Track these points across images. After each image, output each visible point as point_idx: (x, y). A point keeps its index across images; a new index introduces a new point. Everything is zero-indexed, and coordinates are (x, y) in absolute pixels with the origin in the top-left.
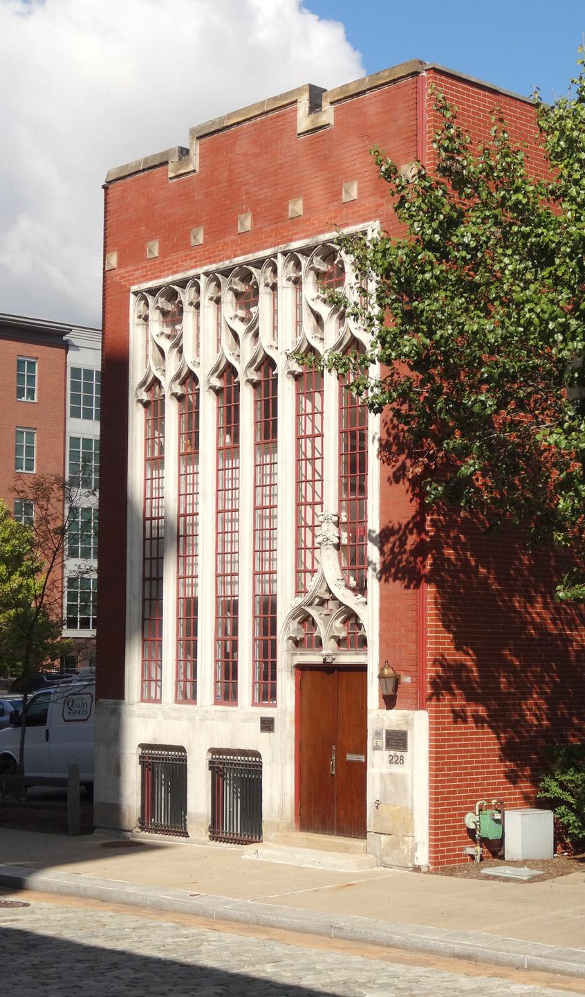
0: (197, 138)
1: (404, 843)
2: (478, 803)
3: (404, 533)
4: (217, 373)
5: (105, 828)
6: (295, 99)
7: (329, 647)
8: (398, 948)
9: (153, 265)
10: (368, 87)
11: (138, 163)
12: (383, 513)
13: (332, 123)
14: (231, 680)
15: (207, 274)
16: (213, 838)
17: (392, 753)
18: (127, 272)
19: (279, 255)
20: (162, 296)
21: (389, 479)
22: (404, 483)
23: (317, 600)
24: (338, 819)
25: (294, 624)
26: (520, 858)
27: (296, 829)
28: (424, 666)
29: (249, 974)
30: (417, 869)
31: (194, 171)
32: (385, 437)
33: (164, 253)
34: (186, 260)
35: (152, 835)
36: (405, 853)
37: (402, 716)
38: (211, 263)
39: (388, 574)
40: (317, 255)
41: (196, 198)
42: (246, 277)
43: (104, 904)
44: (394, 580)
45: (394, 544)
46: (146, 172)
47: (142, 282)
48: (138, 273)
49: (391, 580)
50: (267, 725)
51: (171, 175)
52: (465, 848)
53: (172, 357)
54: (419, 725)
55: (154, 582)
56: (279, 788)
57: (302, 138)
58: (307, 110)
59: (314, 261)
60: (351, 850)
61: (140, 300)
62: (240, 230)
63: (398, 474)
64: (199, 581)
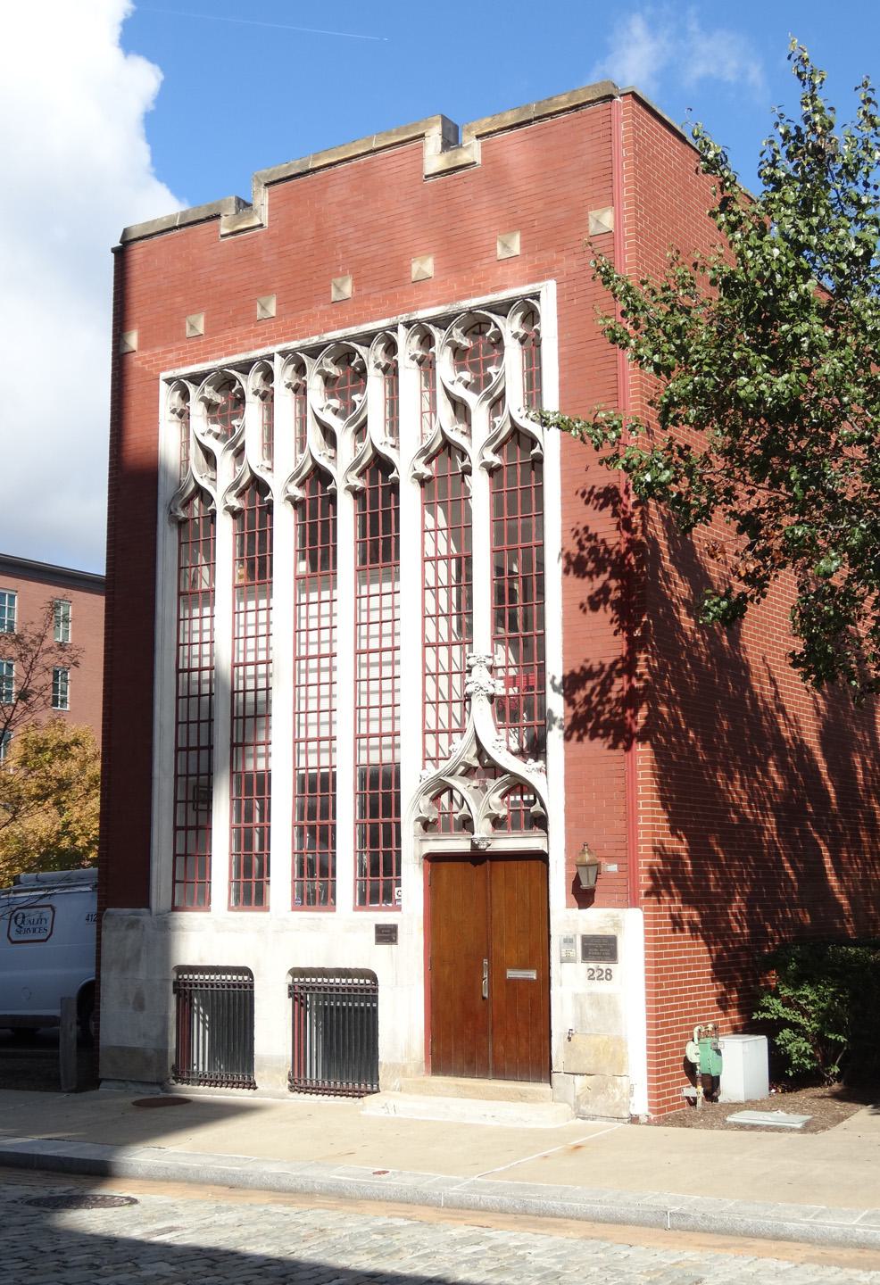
0: (266, 185)
1: (615, 1085)
2: (696, 1029)
3: (609, 676)
4: (297, 480)
5: (119, 1080)
6: (420, 133)
7: (482, 828)
8: (797, 1241)
9: (196, 345)
10: (536, 115)
11: (172, 218)
12: (567, 652)
13: (479, 160)
14: (306, 878)
15: (283, 354)
16: (292, 1089)
17: (592, 965)
18: (154, 355)
19: (401, 327)
20: (209, 384)
21: (582, 606)
22: (606, 611)
23: (462, 769)
24: (494, 1056)
25: (425, 801)
26: (742, 1099)
27: (427, 1071)
28: (635, 849)
29: (419, 1274)
30: (634, 1120)
31: (261, 225)
32: (575, 550)
33: (212, 329)
34: (249, 338)
35: (196, 1087)
36: (617, 1100)
37: (608, 916)
38: (288, 340)
39: (582, 731)
40: (458, 327)
41: (264, 260)
42: (344, 355)
43: (233, 1192)
44: (592, 738)
45: (593, 689)
46: (184, 229)
47: (179, 367)
48: (170, 356)
49: (586, 738)
50: (386, 935)
51: (224, 231)
52: (690, 1091)
53: (225, 460)
54: (630, 926)
55: (204, 753)
56: (402, 1021)
57: (431, 181)
58: (440, 146)
59: (454, 333)
60: (530, 1097)
61: (175, 390)
62: (334, 296)
63: (597, 599)
64: (272, 748)
